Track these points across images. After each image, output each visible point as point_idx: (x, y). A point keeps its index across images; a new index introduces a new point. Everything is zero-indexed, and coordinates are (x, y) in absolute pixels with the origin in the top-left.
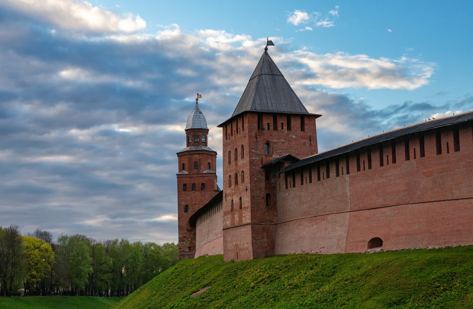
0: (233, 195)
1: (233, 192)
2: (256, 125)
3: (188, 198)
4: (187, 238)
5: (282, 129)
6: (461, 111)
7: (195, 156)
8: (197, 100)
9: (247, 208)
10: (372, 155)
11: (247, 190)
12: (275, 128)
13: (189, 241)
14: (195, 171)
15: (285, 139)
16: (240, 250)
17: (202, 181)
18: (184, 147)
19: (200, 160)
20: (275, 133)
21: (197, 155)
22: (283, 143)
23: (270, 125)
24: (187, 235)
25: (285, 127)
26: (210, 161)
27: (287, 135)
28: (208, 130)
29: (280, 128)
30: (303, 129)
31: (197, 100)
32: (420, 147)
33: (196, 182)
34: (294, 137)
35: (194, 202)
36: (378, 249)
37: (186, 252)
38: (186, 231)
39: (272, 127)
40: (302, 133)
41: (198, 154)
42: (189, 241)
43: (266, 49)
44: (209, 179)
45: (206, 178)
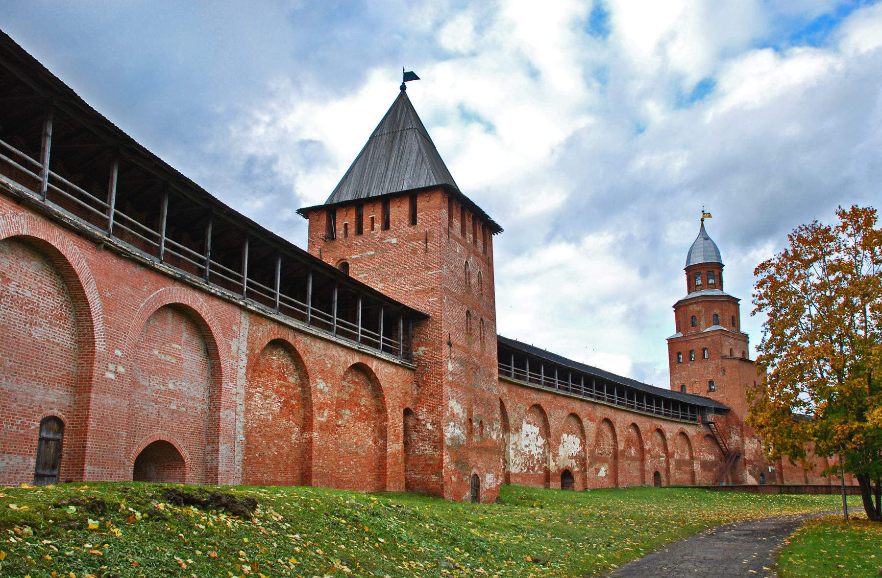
2: (322, 233)
5: (373, 229)
8: (702, 220)
12: (359, 231)
14: (693, 331)
15: (376, 249)
17: (701, 344)
18: (682, 293)
20: (358, 241)
22: (372, 257)
23: (349, 227)
25: (378, 225)
27: (382, 239)
29: (366, 229)
30: (413, 221)
31: (702, 220)
33: (694, 348)
34: (394, 241)
36: (578, 479)
39: (352, 230)
40: (411, 230)
43: (403, 88)
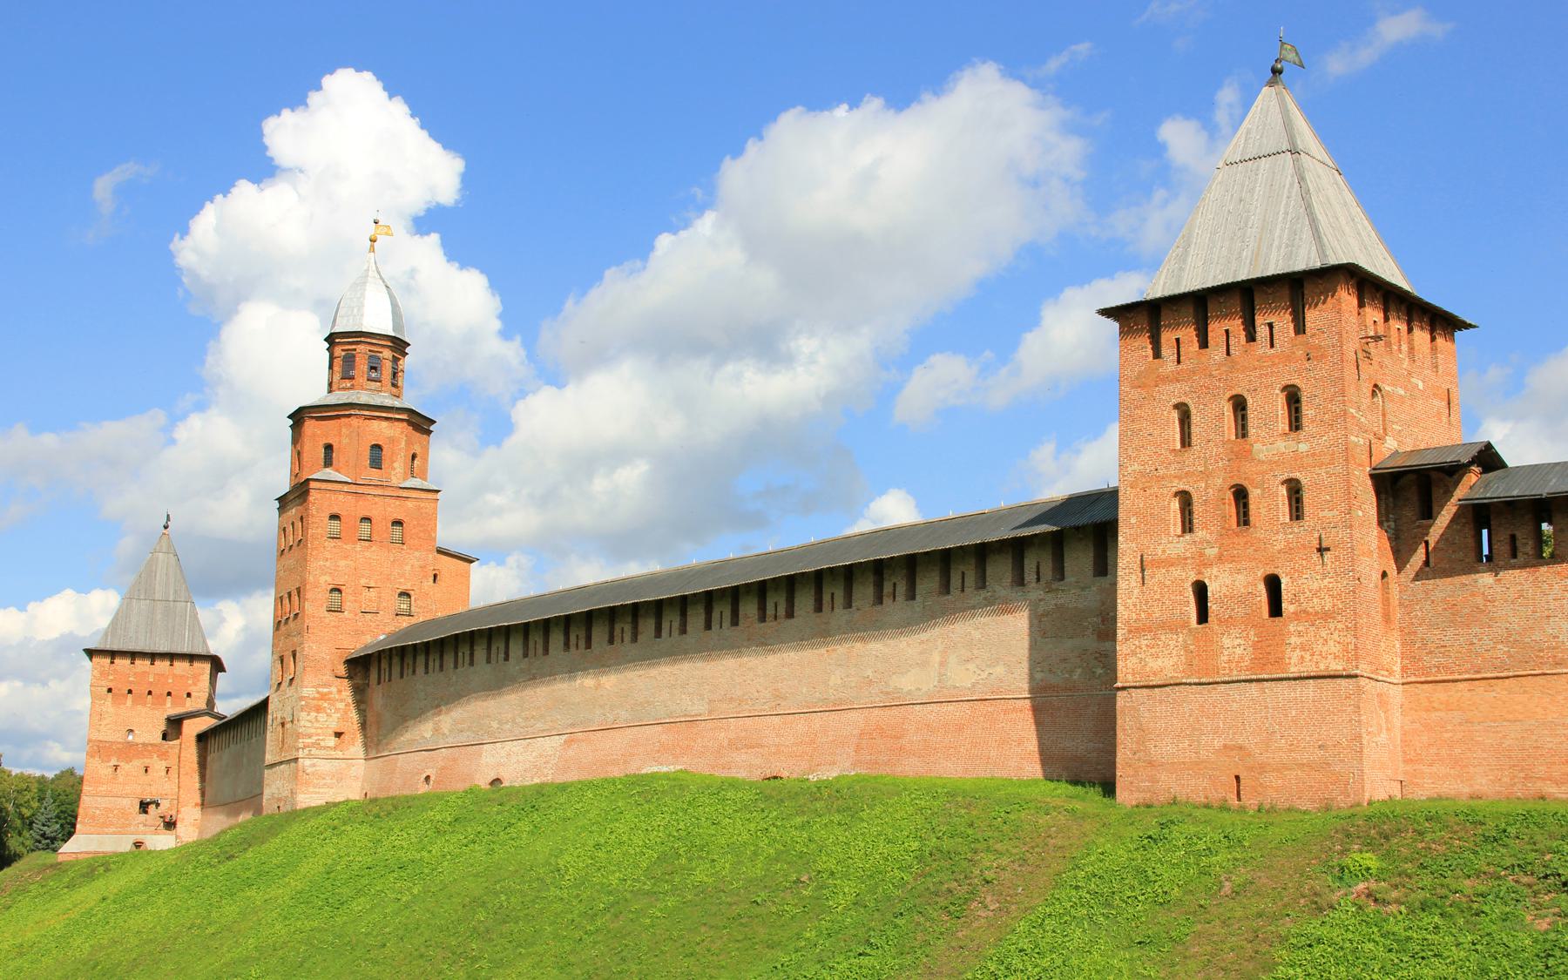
0: (1204, 563)
1: (1212, 552)
3: (342, 563)
4: (332, 701)
6: (551, 745)
7: (375, 423)
9: (1326, 616)
10: (641, 622)
11: (1321, 550)
13: (337, 710)
16: (1263, 768)
17: (395, 510)
19: (392, 440)
21: (385, 424)
24: (334, 689)
25: (1405, 347)
26: (417, 449)
28: (1489, 446)
32: (1054, 569)
35: (363, 582)
37: (325, 748)
38: (329, 677)
41: (387, 419)
42: (337, 710)
44: (419, 508)
45: (410, 504)
